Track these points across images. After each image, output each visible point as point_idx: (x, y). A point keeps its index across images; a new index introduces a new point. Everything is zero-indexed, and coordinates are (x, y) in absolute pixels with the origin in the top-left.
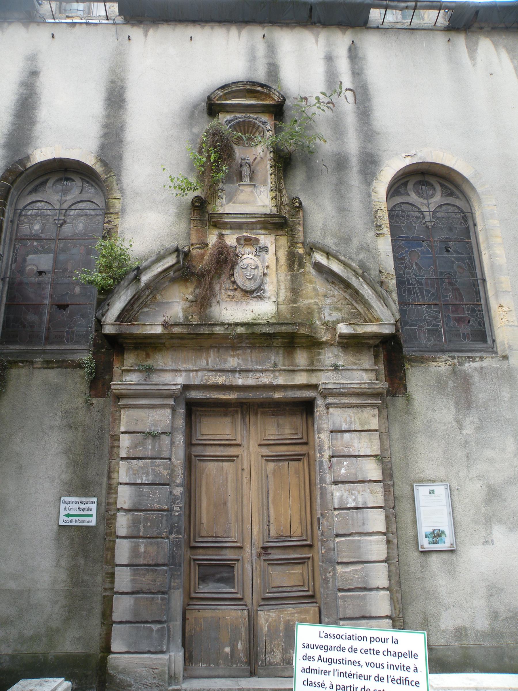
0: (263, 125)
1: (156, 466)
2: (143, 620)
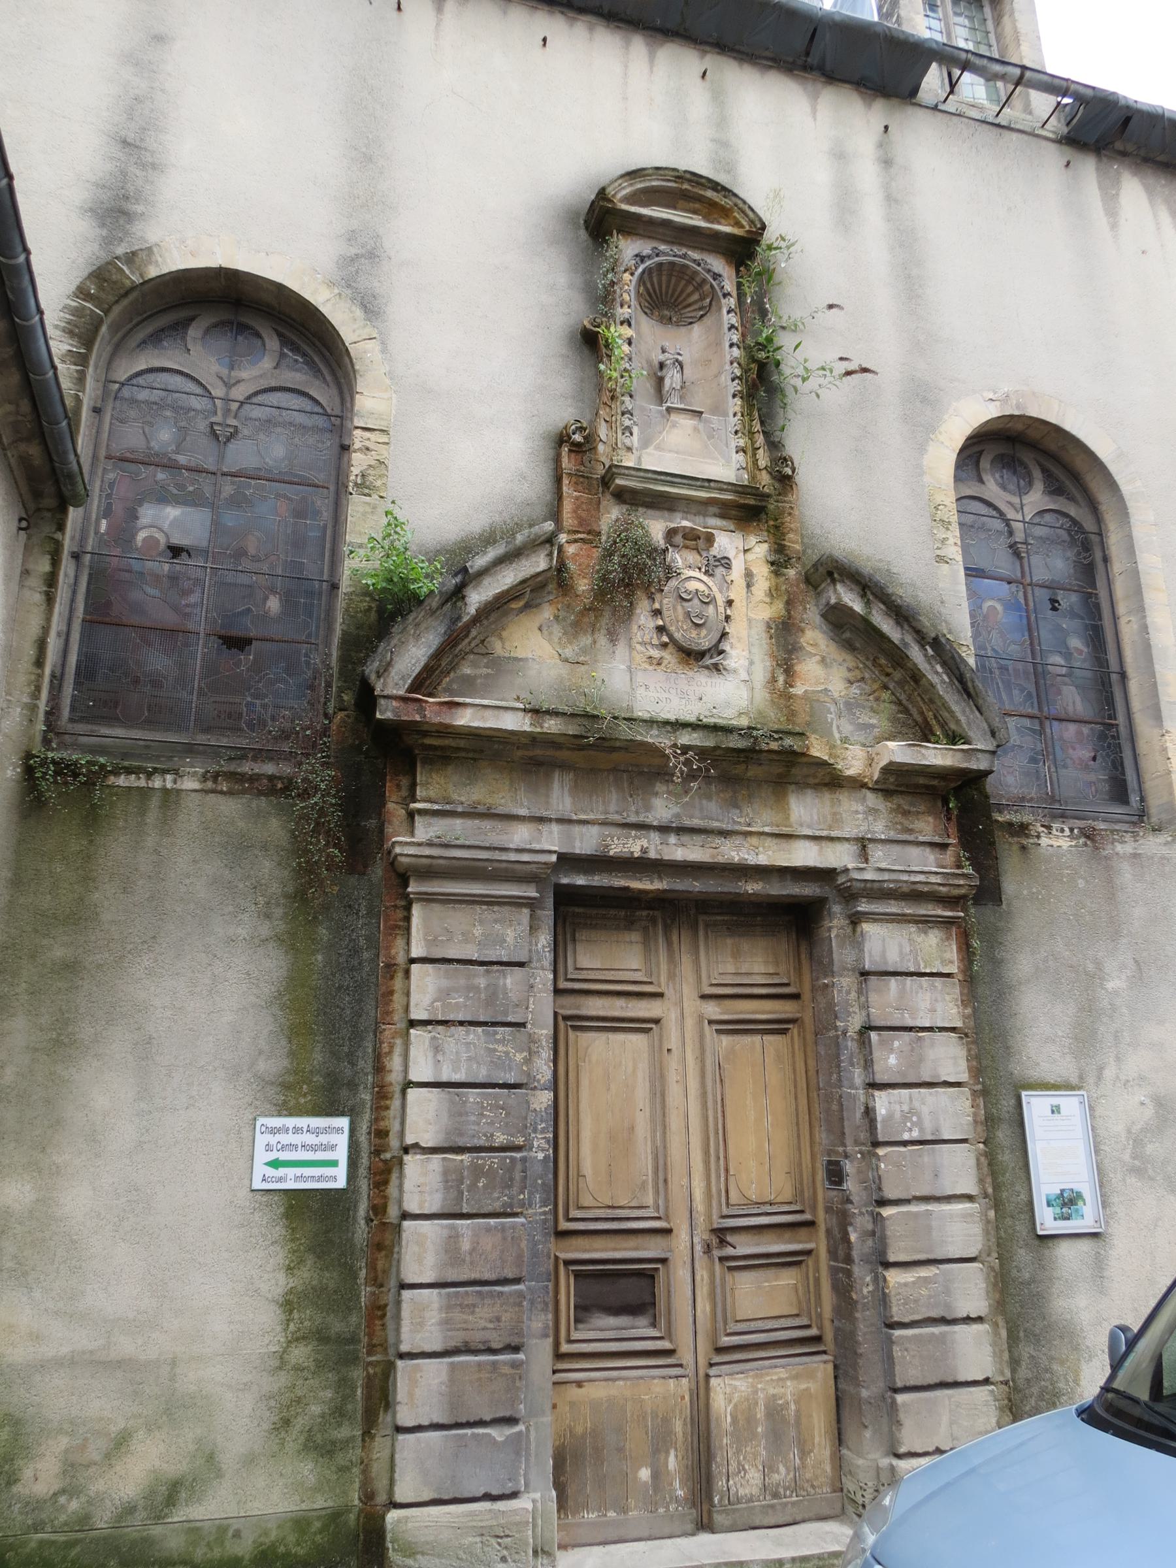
0: (715, 279)
1: (498, 1042)
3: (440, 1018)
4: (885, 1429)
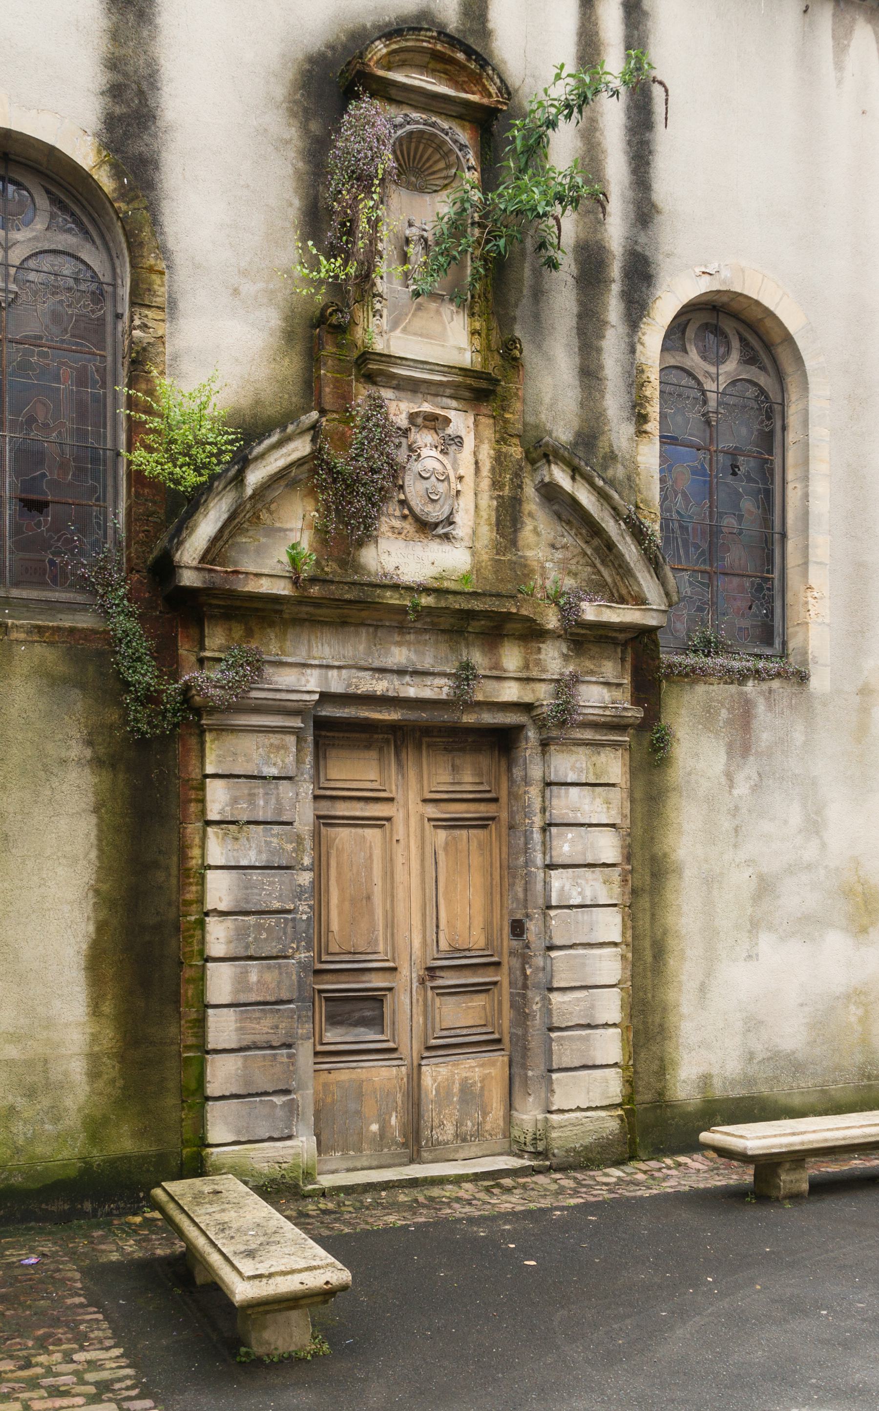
1: (273, 836)
2: (259, 1091)
3: (230, 819)
4: (543, 1095)
